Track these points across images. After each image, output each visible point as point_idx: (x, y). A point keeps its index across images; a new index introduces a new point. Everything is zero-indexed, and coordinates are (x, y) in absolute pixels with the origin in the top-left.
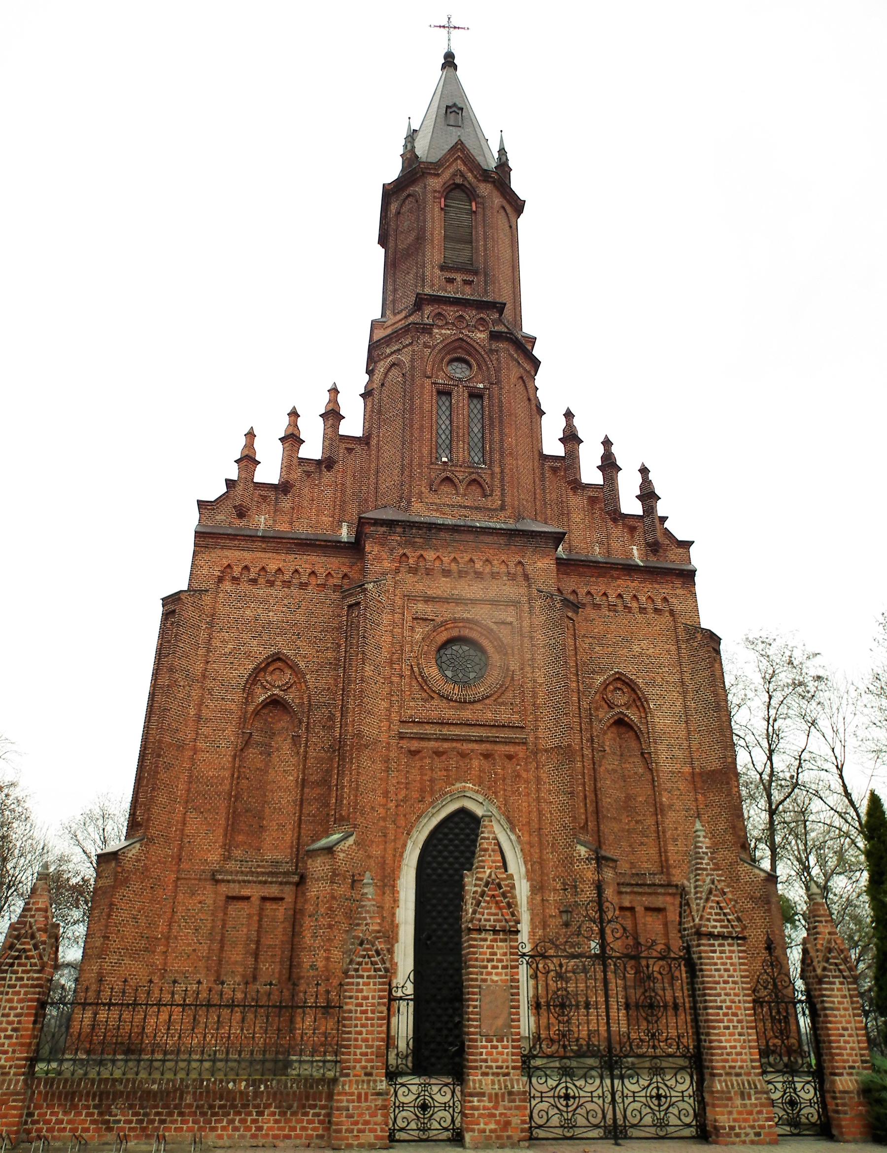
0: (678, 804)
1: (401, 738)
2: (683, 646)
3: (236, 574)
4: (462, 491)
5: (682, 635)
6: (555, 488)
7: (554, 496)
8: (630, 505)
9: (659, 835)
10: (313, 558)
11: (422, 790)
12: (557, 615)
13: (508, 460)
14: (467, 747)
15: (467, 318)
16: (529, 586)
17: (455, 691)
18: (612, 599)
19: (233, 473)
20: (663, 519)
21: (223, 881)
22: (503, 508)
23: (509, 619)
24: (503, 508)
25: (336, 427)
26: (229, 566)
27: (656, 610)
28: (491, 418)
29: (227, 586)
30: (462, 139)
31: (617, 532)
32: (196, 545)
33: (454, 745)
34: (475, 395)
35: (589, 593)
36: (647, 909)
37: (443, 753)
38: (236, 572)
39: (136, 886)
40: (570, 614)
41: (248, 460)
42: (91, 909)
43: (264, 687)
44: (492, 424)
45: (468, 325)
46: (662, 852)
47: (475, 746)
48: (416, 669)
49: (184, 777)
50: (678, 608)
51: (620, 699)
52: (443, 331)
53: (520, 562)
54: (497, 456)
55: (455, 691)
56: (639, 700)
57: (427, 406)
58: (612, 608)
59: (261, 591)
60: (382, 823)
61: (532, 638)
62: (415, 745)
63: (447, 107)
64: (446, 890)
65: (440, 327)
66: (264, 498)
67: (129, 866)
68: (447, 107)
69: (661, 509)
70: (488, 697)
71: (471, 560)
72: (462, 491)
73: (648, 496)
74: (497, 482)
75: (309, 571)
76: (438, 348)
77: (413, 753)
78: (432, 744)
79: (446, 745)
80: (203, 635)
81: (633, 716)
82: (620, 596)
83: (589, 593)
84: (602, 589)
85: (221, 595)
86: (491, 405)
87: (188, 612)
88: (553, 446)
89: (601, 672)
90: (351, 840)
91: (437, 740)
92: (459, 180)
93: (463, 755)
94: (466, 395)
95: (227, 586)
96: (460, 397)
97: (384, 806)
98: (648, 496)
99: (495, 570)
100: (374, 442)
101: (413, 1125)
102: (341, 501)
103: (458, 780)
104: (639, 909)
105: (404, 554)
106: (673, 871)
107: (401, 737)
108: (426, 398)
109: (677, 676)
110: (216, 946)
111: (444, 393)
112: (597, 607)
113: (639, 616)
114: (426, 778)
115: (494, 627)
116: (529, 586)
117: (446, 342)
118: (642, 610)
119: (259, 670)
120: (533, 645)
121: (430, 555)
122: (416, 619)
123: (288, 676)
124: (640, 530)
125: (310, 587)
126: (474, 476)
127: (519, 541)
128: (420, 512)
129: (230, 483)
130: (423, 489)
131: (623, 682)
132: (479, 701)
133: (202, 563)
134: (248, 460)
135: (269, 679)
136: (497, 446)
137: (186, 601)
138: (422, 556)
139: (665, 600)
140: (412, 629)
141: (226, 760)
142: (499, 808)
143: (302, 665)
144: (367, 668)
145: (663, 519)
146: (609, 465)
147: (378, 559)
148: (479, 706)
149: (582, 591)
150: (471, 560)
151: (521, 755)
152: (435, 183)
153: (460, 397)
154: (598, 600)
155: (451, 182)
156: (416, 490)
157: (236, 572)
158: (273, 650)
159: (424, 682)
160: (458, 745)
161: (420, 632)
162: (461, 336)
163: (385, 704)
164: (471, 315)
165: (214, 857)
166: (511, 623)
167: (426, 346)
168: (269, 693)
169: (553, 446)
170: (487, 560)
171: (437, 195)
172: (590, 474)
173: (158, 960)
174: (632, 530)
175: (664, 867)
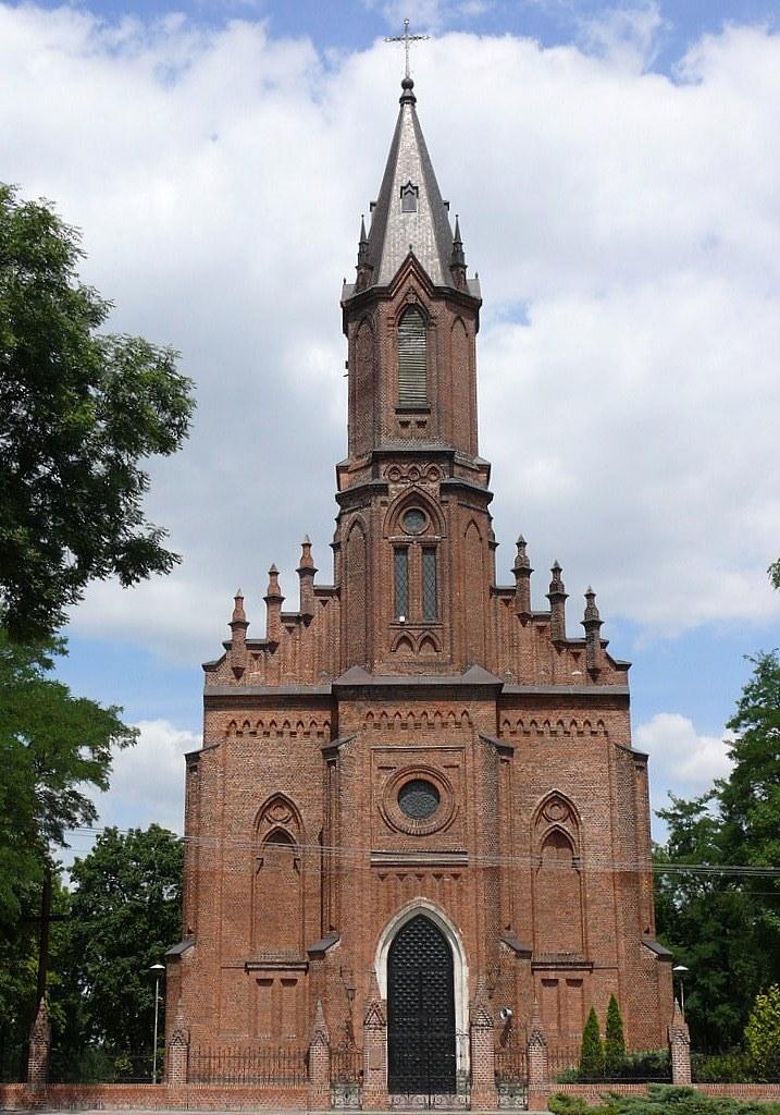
0: (599, 899)
1: (372, 866)
2: (614, 764)
3: (239, 728)
4: (416, 648)
5: (613, 754)
6: (506, 618)
7: (506, 628)
8: (574, 631)
9: (584, 925)
11: (389, 904)
12: (493, 760)
13: (457, 615)
14: (422, 870)
15: (420, 469)
16: (473, 732)
17: (413, 826)
18: (554, 725)
19: (228, 635)
20: (604, 644)
21: (253, 969)
22: (452, 661)
23: (457, 763)
24: (452, 661)
25: (310, 583)
26: (233, 722)
27: (593, 733)
28: (442, 573)
29: (233, 738)
30: (416, 253)
31: (563, 661)
32: (205, 706)
33: (412, 869)
34: (429, 549)
35: (533, 722)
36: (568, 980)
37: (405, 875)
38: (240, 725)
39: (195, 975)
40: (504, 757)
41: (239, 624)
43: (269, 821)
44: (442, 580)
45: (421, 477)
46: (584, 936)
47: (430, 869)
48: (382, 810)
49: (217, 895)
50: (611, 730)
51: (557, 812)
52: (399, 486)
53: (465, 712)
54: (447, 611)
55: (413, 826)
56: (572, 815)
57: (384, 568)
59: (259, 741)
60: (360, 929)
61: (475, 777)
62: (383, 870)
63: (402, 188)
64: (408, 973)
65: (396, 482)
66: (256, 657)
67: (189, 963)
68: (402, 188)
69: (604, 633)
70: (439, 830)
71: (425, 713)
72: (416, 648)
73: (592, 624)
74: (447, 638)
75: (297, 721)
76: (394, 505)
77: (382, 877)
78: (395, 869)
79: (406, 869)
80: (219, 782)
81: (567, 827)
82: (560, 722)
83: (533, 722)
85: (230, 747)
86: (442, 559)
87: (206, 766)
88: (505, 578)
89: (541, 793)
90: (338, 944)
92: (412, 300)
93: (420, 876)
94: (420, 550)
95: (233, 738)
96: (415, 551)
97: (361, 916)
98: (592, 624)
99: (444, 720)
100: (343, 591)
101: (444, 1102)
102: (319, 653)
103: (415, 895)
104: (562, 981)
105: (370, 713)
106: (590, 951)
108: (385, 561)
109: (606, 793)
110: (252, 1013)
111: (401, 549)
112: (540, 733)
113: (576, 739)
114: (392, 894)
115: (444, 771)
116: (473, 732)
117: (402, 497)
118: (580, 733)
119: (265, 809)
120: (475, 784)
121: (391, 711)
122: (382, 768)
123: (286, 812)
124: (583, 656)
125: (298, 735)
126: (427, 633)
128: (384, 675)
130: (383, 649)
131: (557, 799)
132: (431, 833)
133: (212, 721)
134: (239, 624)
135: (272, 814)
136: (447, 602)
137: (203, 758)
138: (384, 713)
139: (601, 722)
140: (378, 777)
141: (247, 881)
142: (446, 914)
143: (296, 802)
144: (343, 814)
145: (604, 644)
146: (557, 596)
147: (349, 718)
150: (425, 713)
151: (464, 874)
152: (387, 309)
153: (415, 551)
154: (541, 727)
155: (405, 302)
156: (377, 651)
157: (240, 725)
158: (274, 792)
159: (388, 822)
160: (416, 869)
161: (385, 777)
162: (415, 489)
163: (359, 840)
164: (423, 467)
165: (244, 951)
166: (457, 766)
167: (384, 503)
168: (274, 826)
169: (505, 578)
170: (438, 712)
171: (391, 322)
172: (539, 603)
173: (214, 1022)
174: (576, 656)
175: (585, 948)
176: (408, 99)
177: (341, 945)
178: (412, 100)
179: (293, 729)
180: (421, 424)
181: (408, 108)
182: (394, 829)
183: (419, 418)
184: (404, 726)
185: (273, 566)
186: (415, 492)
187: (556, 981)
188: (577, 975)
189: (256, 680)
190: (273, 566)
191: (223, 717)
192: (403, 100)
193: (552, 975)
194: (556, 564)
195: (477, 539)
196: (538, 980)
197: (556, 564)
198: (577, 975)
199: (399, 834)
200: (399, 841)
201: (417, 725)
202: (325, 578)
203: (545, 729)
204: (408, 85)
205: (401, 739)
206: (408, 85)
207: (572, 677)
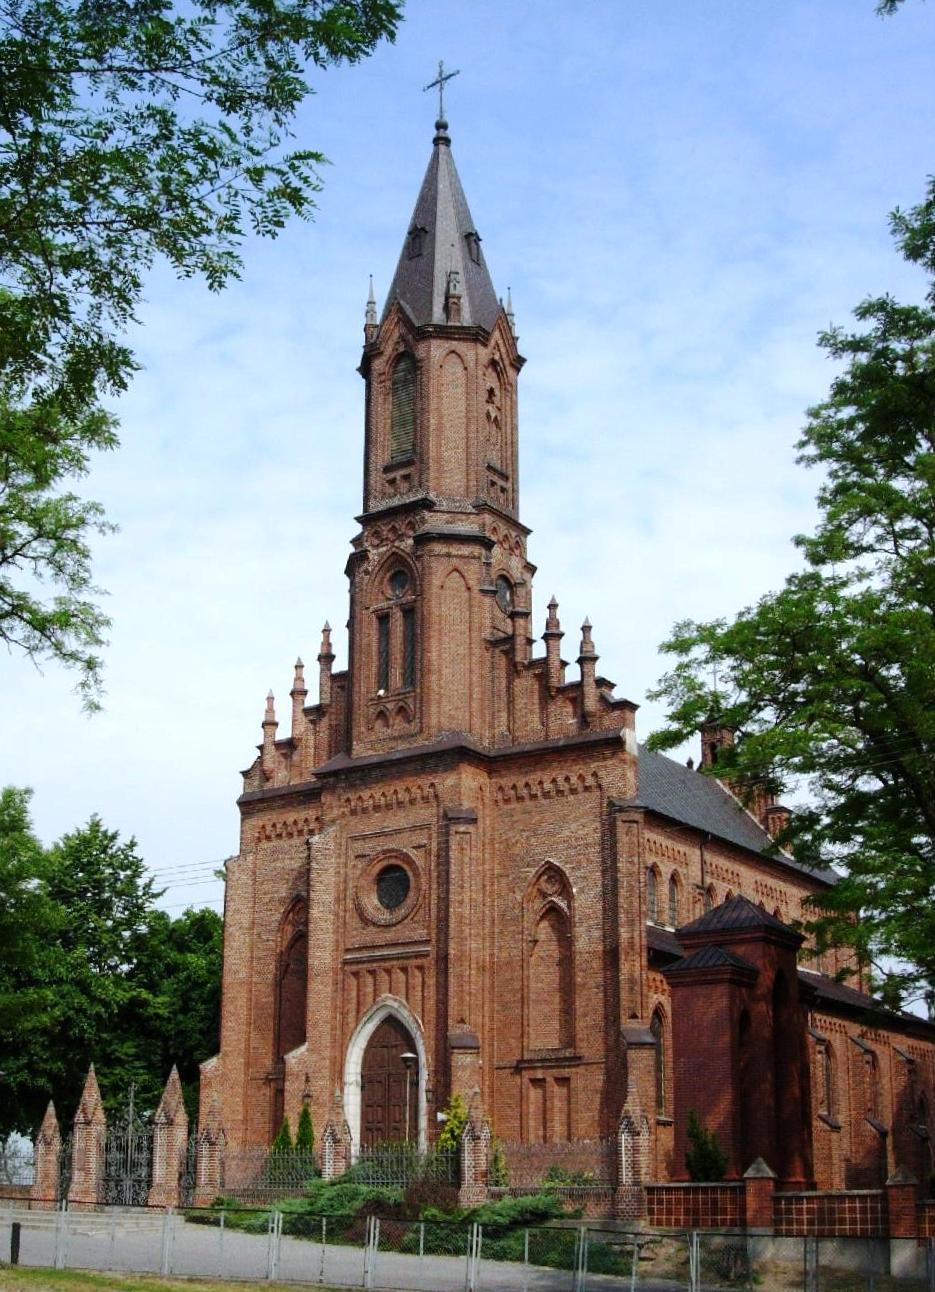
10: (409, 782)
14: (387, 965)
41: (270, 724)
42: (491, 1106)
47: (395, 963)
56: (565, 890)
58: (546, 795)
65: (377, 546)
70: (406, 918)
73: (587, 659)
78: (365, 966)
84: (565, 773)
91: (369, 962)
98: (587, 659)
104: (550, 1079)
107: (346, 963)
112: (533, 797)
116: (438, 806)
121: (366, 794)
126: (401, 704)
127: (432, 762)
129: (261, 748)
138: (360, 797)
148: (399, 927)
149: (521, 783)
176: (442, 141)
177: (308, 1050)
178: (447, 141)
179: (312, 826)
180: (406, 478)
181: (442, 148)
182: (366, 921)
183: (403, 472)
184: (377, 808)
185: (587, 619)
186: (394, 553)
187: (544, 1080)
188: (566, 1072)
189: (281, 778)
190: (587, 619)
191: (257, 821)
192: (437, 141)
193: (539, 1074)
194: (553, 599)
195: (464, 589)
196: (526, 1080)
197: (553, 599)
198: (566, 1072)
199: (371, 928)
200: (371, 935)
201: (388, 807)
202: (340, 665)
203: (524, 792)
204: (441, 126)
205: (376, 822)
206: (441, 126)
207: (564, 721)
